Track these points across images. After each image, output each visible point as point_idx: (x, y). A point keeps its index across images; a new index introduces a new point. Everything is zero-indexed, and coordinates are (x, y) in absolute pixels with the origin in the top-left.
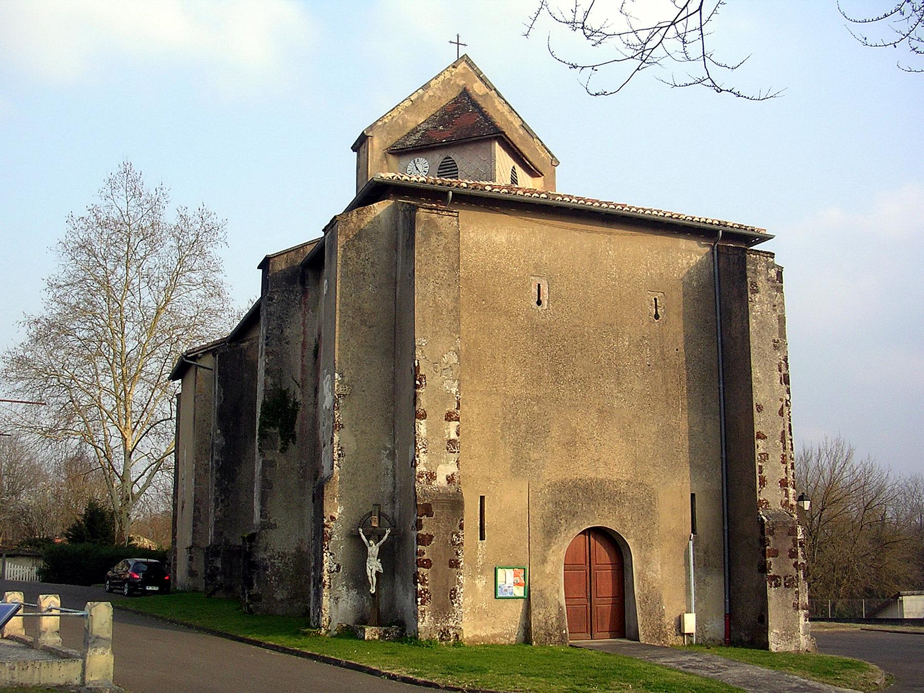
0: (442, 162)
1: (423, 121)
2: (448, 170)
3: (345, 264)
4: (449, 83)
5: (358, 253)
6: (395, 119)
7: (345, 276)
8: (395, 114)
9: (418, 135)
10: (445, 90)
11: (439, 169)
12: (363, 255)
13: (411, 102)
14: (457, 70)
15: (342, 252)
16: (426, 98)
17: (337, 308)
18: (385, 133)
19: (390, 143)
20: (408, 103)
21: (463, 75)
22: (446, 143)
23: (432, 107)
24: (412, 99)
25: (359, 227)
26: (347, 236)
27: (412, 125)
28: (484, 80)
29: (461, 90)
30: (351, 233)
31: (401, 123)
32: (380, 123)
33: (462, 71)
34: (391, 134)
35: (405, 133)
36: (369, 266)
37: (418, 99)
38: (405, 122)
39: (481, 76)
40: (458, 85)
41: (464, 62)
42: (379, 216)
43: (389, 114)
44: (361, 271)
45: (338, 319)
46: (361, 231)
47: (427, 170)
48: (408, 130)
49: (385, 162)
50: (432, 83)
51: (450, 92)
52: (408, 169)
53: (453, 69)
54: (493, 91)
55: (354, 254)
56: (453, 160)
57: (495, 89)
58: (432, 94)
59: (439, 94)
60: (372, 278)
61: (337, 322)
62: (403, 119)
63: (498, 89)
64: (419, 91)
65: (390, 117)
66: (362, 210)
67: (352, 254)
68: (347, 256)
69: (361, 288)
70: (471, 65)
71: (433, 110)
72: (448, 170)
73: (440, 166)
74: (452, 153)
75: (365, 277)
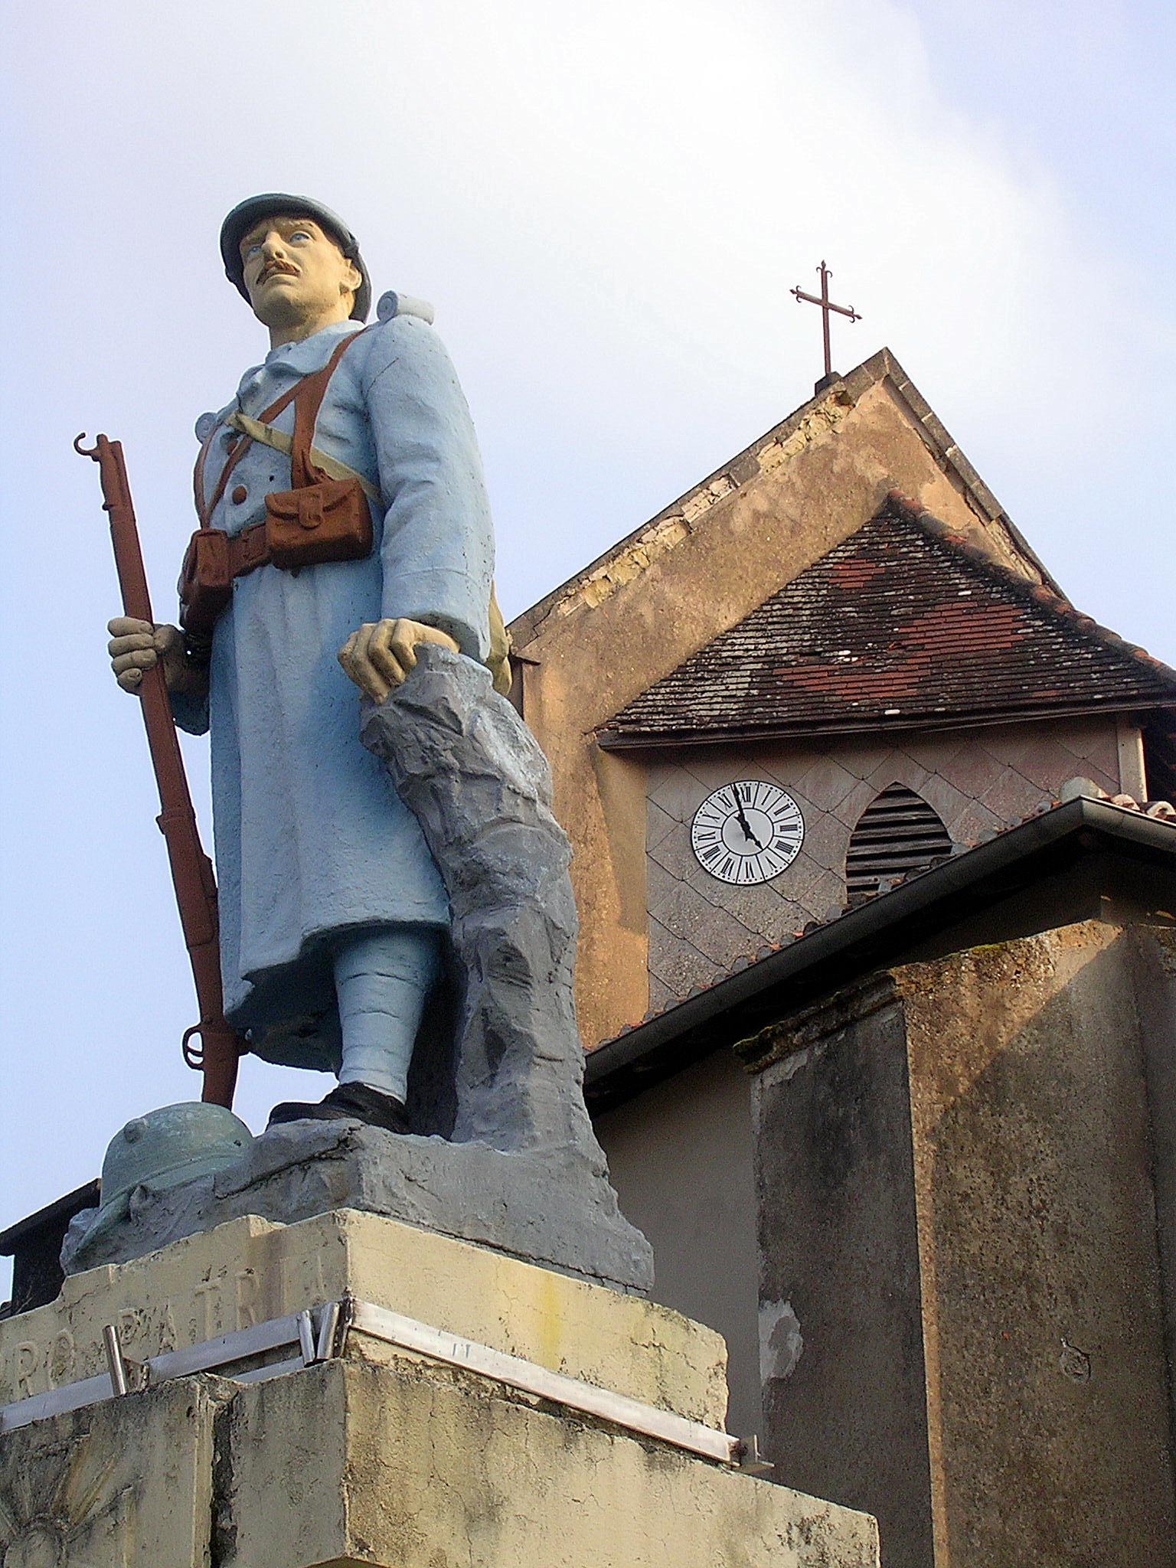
0: (869, 812)
1: (733, 619)
2: (899, 847)
3: (949, 1227)
4: (827, 465)
5: (999, 1173)
6: (623, 598)
7: (952, 1286)
8: (622, 573)
9: (738, 682)
10: (812, 496)
11: (854, 843)
12: (1018, 1183)
13: (682, 534)
14: (854, 417)
15: (931, 1163)
16: (740, 520)
17: (934, 1453)
18: (587, 660)
19: (609, 703)
20: (670, 534)
21: (880, 441)
22: (901, 725)
23: (767, 563)
24: (689, 517)
25: (990, 1040)
26: (947, 1085)
27: (690, 637)
28: (957, 472)
29: (875, 505)
30: (959, 1069)
31: (649, 619)
32: (566, 609)
33: (875, 423)
34: (612, 665)
35: (666, 667)
36: (1046, 1243)
37: (710, 519)
38: (668, 616)
39: (949, 452)
40: (862, 482)
41: (879, 384)
42: (1064, 996)
43: (602, 572)
44: (1019, 1265)
45: (939, 1511)
46: (1000, 1061)
47: (794, 839)
48: (678, 654)
49: (592, 788)
50: (767, 456)
51: (834, 507)
52: (697, 831)
53: (840, 411)
54: (995, 527)
55: (981, 1179)
56: (925, 807)
57: (1003, 520)
58: (763, 505)
59: (794, 512)
60: (1063, 1311)
61: (939, 1530)
62: (658, 602)
63: (1014, 519)
64: (714, 487)
65: (604, 588)
66: (995, 959)
67: (971, 1175)
68: (951, 1179)
69: (1024, 1357)
70: (908, 399)
71: (774, 580)
72: (899, 847)
73: (859, 827)
74: (921, 774)
75: (1037, 1299)
